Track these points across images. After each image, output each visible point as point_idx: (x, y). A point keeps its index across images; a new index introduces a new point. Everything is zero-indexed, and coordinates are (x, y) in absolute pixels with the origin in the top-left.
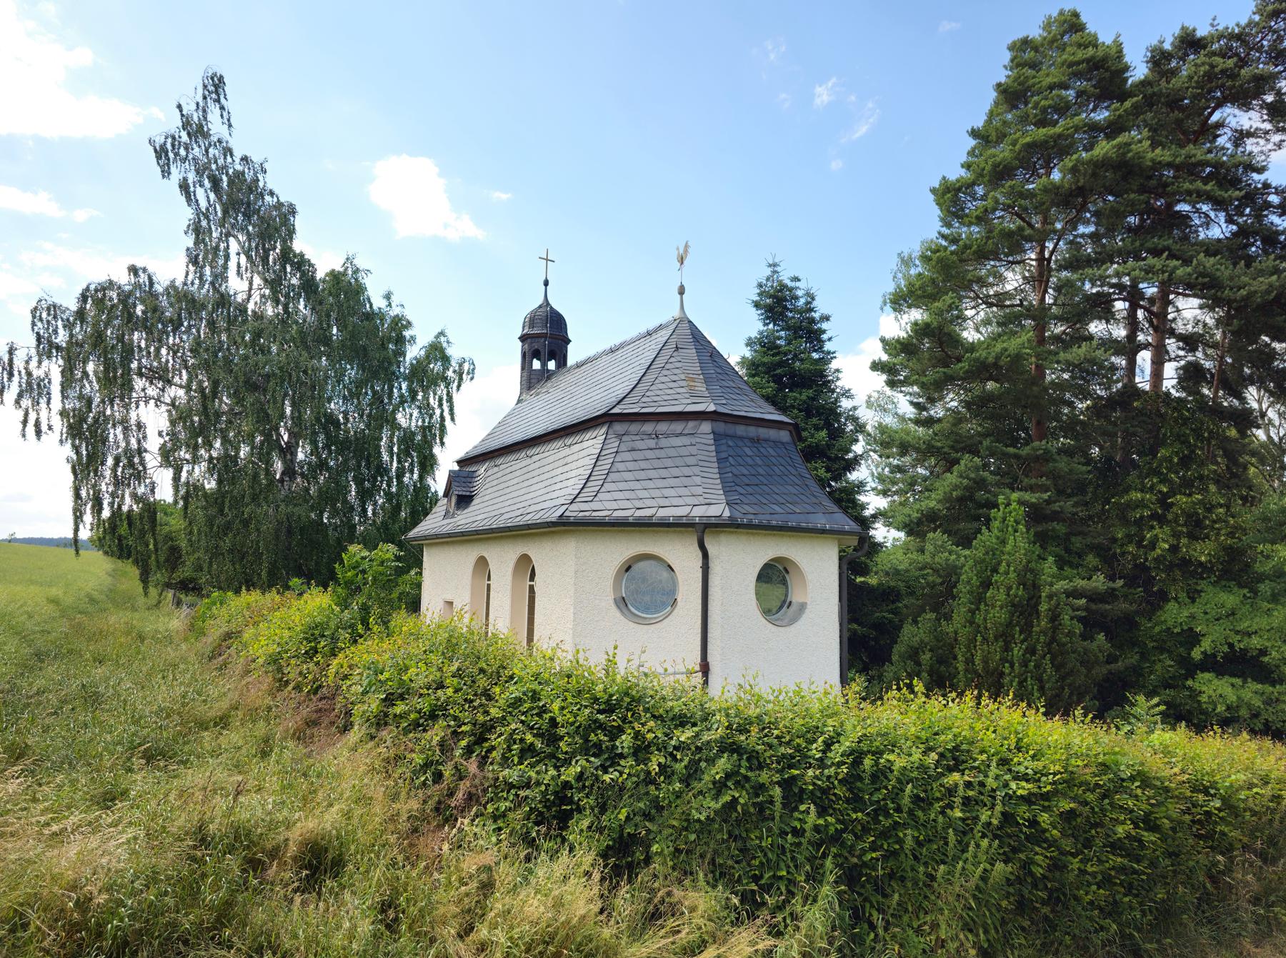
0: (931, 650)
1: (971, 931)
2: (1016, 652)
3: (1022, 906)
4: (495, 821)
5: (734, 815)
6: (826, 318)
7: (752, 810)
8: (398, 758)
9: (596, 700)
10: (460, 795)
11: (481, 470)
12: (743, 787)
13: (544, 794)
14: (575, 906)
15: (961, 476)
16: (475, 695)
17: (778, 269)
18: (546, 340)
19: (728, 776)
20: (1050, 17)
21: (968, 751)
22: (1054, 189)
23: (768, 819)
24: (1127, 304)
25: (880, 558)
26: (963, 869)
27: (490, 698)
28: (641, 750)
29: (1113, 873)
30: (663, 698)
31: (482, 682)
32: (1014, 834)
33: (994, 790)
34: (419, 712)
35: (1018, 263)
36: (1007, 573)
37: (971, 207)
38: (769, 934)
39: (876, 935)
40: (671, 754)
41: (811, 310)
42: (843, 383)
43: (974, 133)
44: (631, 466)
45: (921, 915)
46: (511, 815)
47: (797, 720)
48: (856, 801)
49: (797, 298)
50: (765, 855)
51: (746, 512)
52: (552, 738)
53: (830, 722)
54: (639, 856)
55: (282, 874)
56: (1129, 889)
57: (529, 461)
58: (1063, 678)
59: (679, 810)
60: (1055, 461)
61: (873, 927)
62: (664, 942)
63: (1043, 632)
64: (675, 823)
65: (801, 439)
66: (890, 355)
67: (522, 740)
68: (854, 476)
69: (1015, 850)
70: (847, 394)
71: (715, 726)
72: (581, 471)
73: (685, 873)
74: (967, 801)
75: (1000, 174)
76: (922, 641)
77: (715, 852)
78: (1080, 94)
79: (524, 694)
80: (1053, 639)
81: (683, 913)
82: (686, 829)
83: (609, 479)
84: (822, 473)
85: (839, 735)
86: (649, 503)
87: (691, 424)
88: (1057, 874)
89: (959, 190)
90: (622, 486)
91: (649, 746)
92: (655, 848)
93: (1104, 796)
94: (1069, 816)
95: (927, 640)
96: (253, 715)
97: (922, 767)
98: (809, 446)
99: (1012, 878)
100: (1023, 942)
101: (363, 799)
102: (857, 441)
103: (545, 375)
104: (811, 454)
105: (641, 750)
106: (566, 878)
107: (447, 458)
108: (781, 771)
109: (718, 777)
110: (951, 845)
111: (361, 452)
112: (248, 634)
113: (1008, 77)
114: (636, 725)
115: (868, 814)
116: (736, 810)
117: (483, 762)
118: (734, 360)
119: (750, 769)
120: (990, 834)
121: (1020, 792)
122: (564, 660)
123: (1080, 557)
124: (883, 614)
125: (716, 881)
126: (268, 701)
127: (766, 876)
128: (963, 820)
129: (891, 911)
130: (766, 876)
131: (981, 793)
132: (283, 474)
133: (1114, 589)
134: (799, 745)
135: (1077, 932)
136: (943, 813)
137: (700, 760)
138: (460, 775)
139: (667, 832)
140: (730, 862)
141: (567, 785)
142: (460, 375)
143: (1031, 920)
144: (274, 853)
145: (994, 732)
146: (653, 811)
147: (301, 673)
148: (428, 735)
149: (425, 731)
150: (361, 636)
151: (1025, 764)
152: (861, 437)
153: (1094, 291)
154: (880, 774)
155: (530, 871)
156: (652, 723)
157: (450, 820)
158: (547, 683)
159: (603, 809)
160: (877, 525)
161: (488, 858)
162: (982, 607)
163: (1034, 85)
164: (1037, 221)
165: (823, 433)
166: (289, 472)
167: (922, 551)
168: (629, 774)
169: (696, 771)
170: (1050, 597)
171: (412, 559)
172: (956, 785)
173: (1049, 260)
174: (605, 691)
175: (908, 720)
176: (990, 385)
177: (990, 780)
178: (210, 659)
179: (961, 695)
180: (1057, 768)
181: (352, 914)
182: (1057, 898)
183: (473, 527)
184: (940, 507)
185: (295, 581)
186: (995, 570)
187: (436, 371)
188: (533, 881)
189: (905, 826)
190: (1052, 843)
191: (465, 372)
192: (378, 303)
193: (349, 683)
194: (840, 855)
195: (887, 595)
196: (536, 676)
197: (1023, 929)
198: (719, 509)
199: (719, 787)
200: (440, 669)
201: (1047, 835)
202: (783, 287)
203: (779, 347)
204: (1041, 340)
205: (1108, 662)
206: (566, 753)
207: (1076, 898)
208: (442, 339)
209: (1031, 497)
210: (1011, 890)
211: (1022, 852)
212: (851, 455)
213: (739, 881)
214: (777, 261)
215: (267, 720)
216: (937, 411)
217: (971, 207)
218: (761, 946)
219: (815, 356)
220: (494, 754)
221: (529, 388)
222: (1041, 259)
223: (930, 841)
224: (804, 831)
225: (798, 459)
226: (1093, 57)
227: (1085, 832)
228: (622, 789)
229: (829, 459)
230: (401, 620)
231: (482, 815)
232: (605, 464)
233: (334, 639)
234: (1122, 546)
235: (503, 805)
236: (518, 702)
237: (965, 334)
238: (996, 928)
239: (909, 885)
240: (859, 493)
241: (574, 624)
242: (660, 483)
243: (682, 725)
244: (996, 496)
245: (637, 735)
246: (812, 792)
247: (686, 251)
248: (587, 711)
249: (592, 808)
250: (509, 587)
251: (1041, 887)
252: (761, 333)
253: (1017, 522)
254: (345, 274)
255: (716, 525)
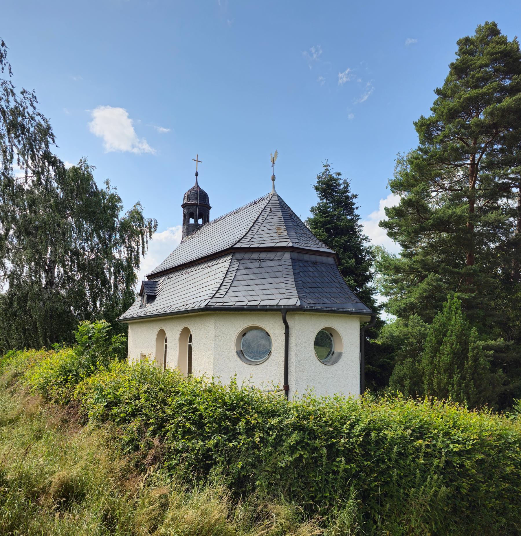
0: (410, 379)
1: (428, 523)
2: (455, 379)
3: (455, 510)
4: (169, 471)
5: (301, 464)
6: (355, 196)
7: (311, 461)
8: (114, 438)
9: (225, 403)
10: (149, 457)
11: (161, 281)
12: (306, 449)
13: (196, 455)
14: (213, 514)
15: (428, 284)
16: (158, 402)
17: (329, 168)
18: (197, 208)
19: (298, 443)
20: (480, 26)
21: (428, 428)
22: (480, 125)
23: (319, 466)
24: (518, 189)
25: (383, 330)
26: (424, 490)
27: (166, 404)
28: (250, 430)
29: (504, 492)
30: (263, 403)
31: (161, 395)
32: (451, 471)
33: (441, 449)
34: (126, 413)
35: (460, 166)
36: (451, 336)
37: (438, 134)
38: (319, 526)
39: (377, 527)
40: (267, 432)
41: (347, 191)
42: (364, 233)
43: (438, 92)
44: (245, 277)
45: (402, 516)
46: (178, 467)
47: (335, 412)
48: (367, 456)
49: (339, 185)
50: (318, 485)
51: (309, 302)
52: (200, 425)
53: (353, 414)
54: (249, 487)
55: (48, 501)
56: (512, 501)
57: (187, 275)
58: (480, 393)
59: (271, 462)
60: (479, 276)
61: (375, 522)
62: (263, 532)
63: (470, 368)
64: (269, 469)
65: (340, 264)
66: (389, 217)
67: (184, 426)
68: (370, 285)
69: (451, 481)
70: (366, 239)
71: (291, 416)
72: (217, 280)
73: (274, 496)
74: (426, 455)
75: (452, 115)
76: (405, 373)
77: (291, 484)
78: (497, 70)
79: (185, 401)
80: (475, 372)
81: (273, 517)
82: (275, 472)
83: (233, 285)
84: (352, 282)
85: (358, 420)
86: (256, 298)
87: (279, 254)
88: (474, 493)
89: (429, 125)
90: (240, 288)
91: (254, 428)
92: (257, 483)
93: (500, 452)
94: (481, 462)
95: (408, 373)
96: (31, 416)
97: (403, 437)
98: (345, 268)
99: (450, 495)
100: (456, 529)
101: (95, 462)
102: (371, 265)
103: (197, 227)
104: (346, 272)
105: (250, 430)
106: (208, 500)
107: (141, 275)
108: (326, 440)
109: (292, 444)
110: (418, 478)
111: (92, 270)
112: (27, 374)
113: (457, 60)
114: (247, 417)
115: (373, 462)
116: (302, 462)
117: (161, 441)
118: (303, 219)
119: (310, 439)
120: (438, 472)
121: (455, 449)
122: (207, 383)
123: (491, 328)
124: (384, 359)
125: (291, 499)
126: (40, 409)
127: (318, 496)
128: (424, 464)
129: (385, 513)
130: (318, 496)
131: (435, 451)
132: (47, 284)
133: (508, 346)
134: (336, 426)
135: (484, 523)
136: (414, 461)
137: (282, 435)
138: (149, 446)
139: (264, 474)
140: (298, 489)
141: (209, 450)
142: (150, 228)
143: (460, 517)
144: (44, 490)
145: (442, 418)
146: (257, 463)
147: (58, 393)
148: (130, 426)
149: (129, 423)
150: (92, 373)
151: (460, 436)
152: (373, 263)
153: (500, 182)
154: (381, 441)
155: (188, 497)
156: (256, 415)
157: (144, 471)
158: (198, 395)
159: (229, 462)
160: (381, 312)
161: (165, 490)
162: (437, 354)
163: (471, 65)
164: (471, 142)
165: (353, 261)
166: (50, 283)
167: (406, 325)
168: (243, 443)
169: (280, 441)
170: (474, 349)
171: (119, 328)
172: (421, 446)
173: (477, 164)
174: (230, 399)
175: (395, 412)
176: (445, 235)
177: (439, 443)
178: (7, 387)
179: (423, 399)
180: (475, 437)
181: (87, 523)
182: (473, 506)
183: (156, 312)
184: (416, 301)
185: (56, 345)
186: (445, 335)
187: (136, 228)
188: (190, 502)
189: (393, 468)
190: (471, 477)
191: (152, 228)
192: (101, 186)
193: (86, 398)
194: (358, 485)
195: (387, 349)
196: (192, 392)
197: (456, 522)
198: (294, 301)
199: (293, 449)
200: (137, 389)
201: (469, 472)
202: (332, 179)
203: (329, 212)
204: (472, 209)
205: (504, 384)
206: (208, 433)
207: (484, 506)
208: (138, 207)
209: (466, 296)
210: (450, 502)
211: (455, 481)
212: (368, 273)
213: (303, 499)
214: (328, 163)
215: (39, 420)
216: (416, 249)
217: (438, 134)
218: (314, 533)
219: (349, 217)
220: (168, 434)
221: (188, 234)
222: (473, 164)
223: (407, 476)
224: (339, 472)
225: (338, 274)
226: (504, 50)
227: (489, 471)
228: (239, 451)
229: (356, 275)
230: (115, 364)
231: (162, 468)
232: (231, 277)
233: (77, 375)
234: (513, 321)
235: (174, 462)
236: (181, 406)
237: (430, 206)
238: (441, 522)
239: (395, 499)
240: (372, 294)
241: (214, 363)
242: (262, 287)
243: (273, 416)
244: (446, 295)
245: (248, 422)
246: (343, 451)
247: (276, 156)
248: (220, 410)
249: (223, 462)
250: (178, 346)
251: (465, 499)
252: (319, 204)
253: (457, 309)
254: (80, 169)
255: (293, 310)
